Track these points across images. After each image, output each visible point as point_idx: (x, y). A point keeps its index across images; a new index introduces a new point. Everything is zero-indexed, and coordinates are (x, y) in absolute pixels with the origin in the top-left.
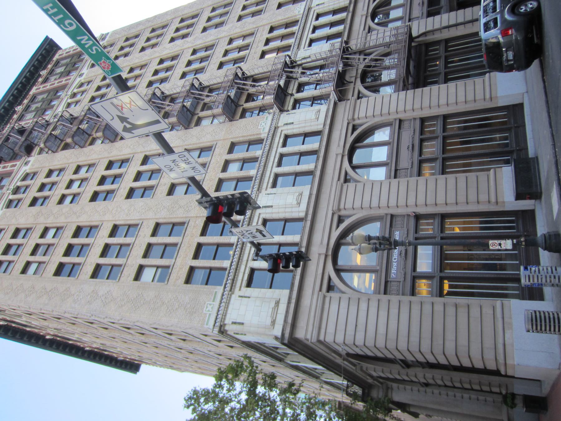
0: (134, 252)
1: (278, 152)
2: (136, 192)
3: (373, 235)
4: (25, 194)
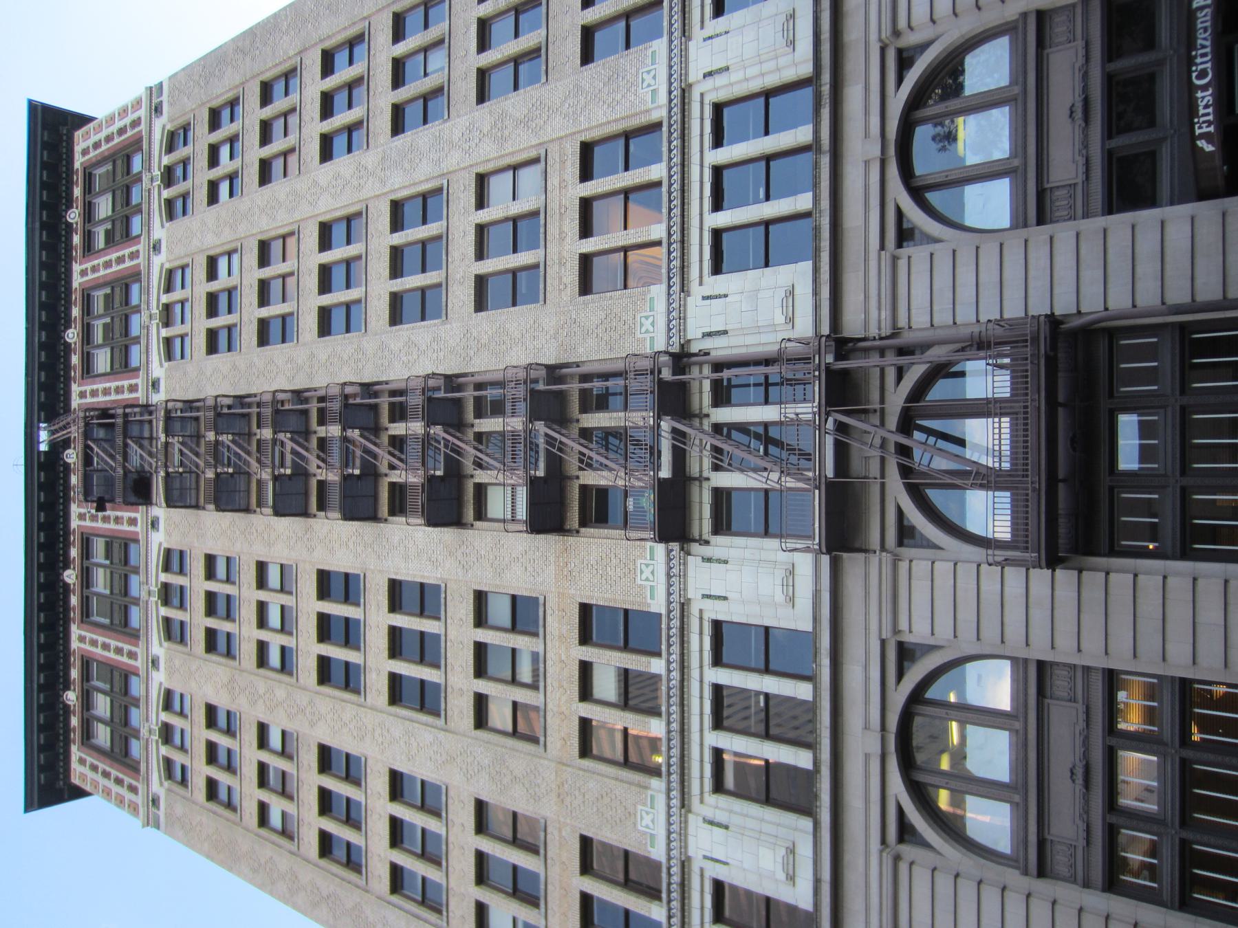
0: (455, 254)
1: (706, 164)
2: (409, 111)
3: (992, 318)
4: (190, 181)
